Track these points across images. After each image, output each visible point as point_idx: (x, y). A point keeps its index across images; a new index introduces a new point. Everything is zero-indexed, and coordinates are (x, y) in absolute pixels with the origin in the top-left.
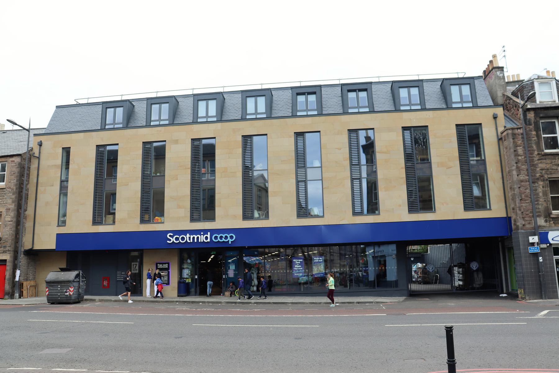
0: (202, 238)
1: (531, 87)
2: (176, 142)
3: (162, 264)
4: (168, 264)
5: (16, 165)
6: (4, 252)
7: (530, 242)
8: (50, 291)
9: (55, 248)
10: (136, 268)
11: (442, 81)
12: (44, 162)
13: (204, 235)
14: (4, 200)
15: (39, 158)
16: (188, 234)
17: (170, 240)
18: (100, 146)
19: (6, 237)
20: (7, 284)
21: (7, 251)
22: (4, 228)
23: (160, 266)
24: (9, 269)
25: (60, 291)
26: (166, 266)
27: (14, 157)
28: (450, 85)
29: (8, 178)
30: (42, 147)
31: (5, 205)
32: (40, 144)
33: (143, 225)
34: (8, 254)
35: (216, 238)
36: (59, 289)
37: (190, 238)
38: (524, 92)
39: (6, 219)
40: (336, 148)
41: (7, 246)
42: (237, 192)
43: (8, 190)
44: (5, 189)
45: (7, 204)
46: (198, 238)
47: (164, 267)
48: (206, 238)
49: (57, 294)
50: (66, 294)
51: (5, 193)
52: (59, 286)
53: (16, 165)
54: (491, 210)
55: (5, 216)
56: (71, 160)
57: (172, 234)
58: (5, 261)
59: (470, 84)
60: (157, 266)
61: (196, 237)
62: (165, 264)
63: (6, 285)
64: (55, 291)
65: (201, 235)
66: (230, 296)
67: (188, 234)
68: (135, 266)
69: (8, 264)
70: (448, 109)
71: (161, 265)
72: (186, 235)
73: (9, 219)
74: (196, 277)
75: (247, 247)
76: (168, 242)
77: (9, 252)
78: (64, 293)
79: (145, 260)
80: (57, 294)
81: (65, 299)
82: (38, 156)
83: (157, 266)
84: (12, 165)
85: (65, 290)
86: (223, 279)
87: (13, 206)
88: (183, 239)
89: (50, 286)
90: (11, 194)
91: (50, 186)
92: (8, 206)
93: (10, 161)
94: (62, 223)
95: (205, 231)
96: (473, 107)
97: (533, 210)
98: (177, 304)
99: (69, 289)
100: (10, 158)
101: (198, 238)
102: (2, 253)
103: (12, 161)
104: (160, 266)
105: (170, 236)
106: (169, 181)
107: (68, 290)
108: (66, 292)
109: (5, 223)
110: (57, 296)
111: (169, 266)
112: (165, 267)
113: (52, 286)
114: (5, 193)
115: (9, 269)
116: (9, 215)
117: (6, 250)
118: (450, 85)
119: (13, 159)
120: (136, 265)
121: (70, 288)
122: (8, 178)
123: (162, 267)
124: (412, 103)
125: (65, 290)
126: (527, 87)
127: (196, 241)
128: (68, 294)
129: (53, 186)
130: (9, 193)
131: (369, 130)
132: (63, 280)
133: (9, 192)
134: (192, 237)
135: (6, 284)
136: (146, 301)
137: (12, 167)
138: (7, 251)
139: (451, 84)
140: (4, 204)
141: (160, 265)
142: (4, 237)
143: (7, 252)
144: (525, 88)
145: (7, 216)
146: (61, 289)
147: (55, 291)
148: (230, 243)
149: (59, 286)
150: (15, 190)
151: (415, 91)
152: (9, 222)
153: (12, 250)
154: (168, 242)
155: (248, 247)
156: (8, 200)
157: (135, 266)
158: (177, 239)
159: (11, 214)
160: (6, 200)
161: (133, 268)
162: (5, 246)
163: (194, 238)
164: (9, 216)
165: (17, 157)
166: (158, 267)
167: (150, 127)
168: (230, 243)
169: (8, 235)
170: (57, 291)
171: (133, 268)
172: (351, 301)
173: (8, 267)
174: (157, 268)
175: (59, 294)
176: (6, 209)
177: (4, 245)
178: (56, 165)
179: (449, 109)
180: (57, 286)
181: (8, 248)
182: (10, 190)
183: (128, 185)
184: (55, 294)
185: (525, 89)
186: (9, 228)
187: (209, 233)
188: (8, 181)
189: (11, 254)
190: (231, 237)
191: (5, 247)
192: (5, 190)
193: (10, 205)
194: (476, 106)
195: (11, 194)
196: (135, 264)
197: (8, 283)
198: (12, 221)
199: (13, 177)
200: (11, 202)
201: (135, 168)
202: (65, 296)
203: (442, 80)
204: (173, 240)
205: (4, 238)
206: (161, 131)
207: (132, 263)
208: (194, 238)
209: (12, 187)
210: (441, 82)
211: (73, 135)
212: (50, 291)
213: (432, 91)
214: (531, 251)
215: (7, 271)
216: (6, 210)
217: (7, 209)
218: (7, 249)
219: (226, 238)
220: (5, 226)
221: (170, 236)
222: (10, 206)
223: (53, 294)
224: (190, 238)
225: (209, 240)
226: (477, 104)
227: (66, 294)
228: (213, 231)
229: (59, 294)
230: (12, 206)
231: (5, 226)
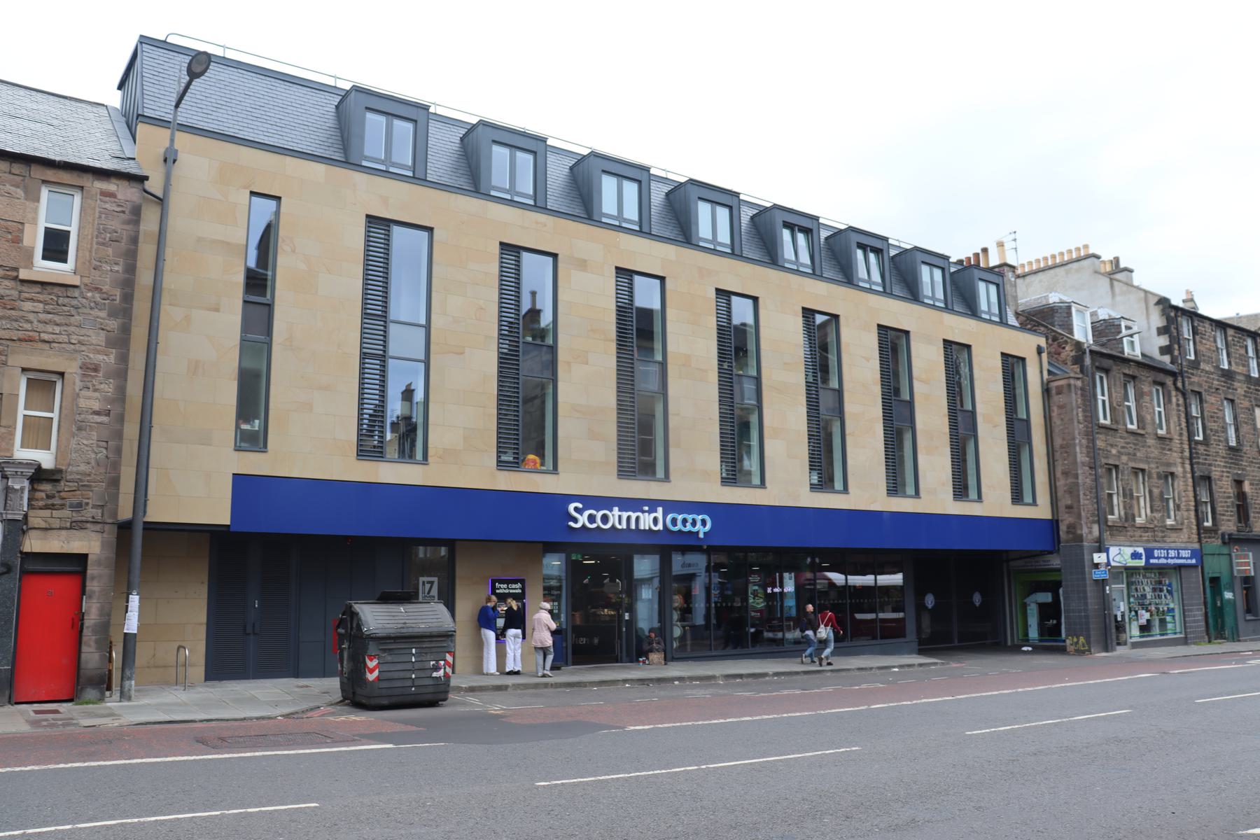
0: (646, 521)
1: (1067, 313)
2: (582, 264)
3: (508, 582)
4: (522, 582)
5: (123, 212)
6: (77, 525)
7: (1096, 561)
8: (385, 668)
9: (229, 523)
10: (431, 594)
11: (469, 130)
12: (181, 222)
13: (650, 512)
14: (72, 329)
15: (161, 201)
16: (616, 509)
17: (576, 520)
18: (376, 221)
19: (83, 468)
20: (92, 644)
21: (87, 522)
22: (73, 435)
23: (502, 589)
24: (97, 589)
25: (417, 666)
26: (516, 588)
27: (114, 180)
28: (367, 108)
29: (90, 252)
30: (177, 170)
31: (76, 351)
32: (169, 159)
33: (506, 473)
34: (93, 534)
35: (674, 521)
36: (413, 660)
37: (620, 517)
38: (1056, 318)
39: (83, 403)
40: (863, 357)
41: (87, 504)
42: (710, 419)
43: (89, 294)
44: (76, 290)
45: (83, 348)
46: (637, 519)
47: (511, 591)
48: (655, 521)
49: (407, 675)
50: (435, 674)
51: (74, 302)
52: (414, 651)
53: (123, 212)
54: (1037, 505)
55: (77, 390)
56: (283, 241)
57: (580, 506)
58: (82, 558)
59: (415, 121)
60: (494, 589)
61: (634, 516)
62: (515, 581)
63: (84, 649)
64: (400, 667)
65: (643, 512)
66: (663, 662)
67: (616, 509)
68: (428, 586)
69: (91, 570)
70: (884, 294)
71: (505, 586)
72: (611, 511)
73: (96, 406)
74: (627, 616)
75: (705, 547)
76: (571, 524)
77: (98, 527)
78: (427, 673)
79: (460, 572)
80: (407, 675)
81: (431, 690)
82: (160, 194)
83: (494, 589)
84: (107, 206)
85: (432, 663)
86: (624, 624)
87: (112, 357)
88: (605, 519)
89: (384, 650)
90: (103, 314)
91: (209, 309)
92: (91, 356)
93: (99, 191)
94: (254, 441)
95: (653, 504)
96: (414, 177)
97: (1098, 515)
98: (628, 687)
99: (445, 660)
100: (97, 180)
101: (637, 519)
102: (67, 529)
103: (104, 194)
104: (502, 589)
105: (576, 509)
106: (569, 363)
107: (442, 663)
108: (437, 669)
109: (78, 417)
110: (409, 683)
111: (523, 589)
112: (514, 591)
113: (390, 649)
114: (74, 302)
115: (97, 589)
116: (96, 390)
117: (84, 519)
118: (367, 108)
119: (111, 186)
120: (432, 583)
121: (447, 655)
122: (90, 252)
123: (507, 591)
124: (517, 190)
125: (432, 663)
126: (1059, 311)
127: (633, 526)
128: (441, 673)
129: (217, 310)
130: (91, 308)
131: (527, 254)
132: (425, 630)
133: (92, 305)
134: (625, 515)
135: (89, 646)
136: (552, 684)
137: (107, 213)
138: (87, 522)
139: (924, 261)
140: (72, 346)
141: (502, 586)
142: (75, 469)
143: (88, 525)
144: (1057, 312)
145: (84, 393)
146: (419, 659)
147: (400, 667)
148: (701, 535)
149: (414, 651)
150: (118, 302)
151: (404, 129)
152: (96, 417)
153: (110, 521)
154: (571, 524)
155: (708, 546)
156: (90, 332)
157: (428, 586)
158: (592, 519)
159: (102, 386)
160: (83, 332)
161: (423, 593)
162: (80, 505)
163: (629, 518)
164: (97, 394)
165: (125, 183)
166: (497, 591)
167: (647, 236)
168: (701, 535)
169: (93, 462)
170: (409, 666)
171: (423, 593)
172: (710, 673)
173: (95, 583)
174: (493, 592)
175: (413, 676)
176: (79, 363)
177: (75, 501)
178: (228, 244)
179: (743, 259)
180: (407, 651)
181: (89, 513)
182: (97, 296)
183: (462, 353)
184: (402, 675)
185: (1057, 315)
186: (95, 438)
187: (660, 510)
188: (90, 262)
189: (105, 535)
190: (704, 523)
191: (79, 506)
192: (76, 293)
193: (98, 352)
194: (424, 178)
195: (103, 314)
196: (428, 582)
197: (97, 642)
198: (108, 413)
199: (110, 251)
200: (104, 344)
201: (482, 309)
202: (429, 682)
203: (469, 128)
204: (583, 520)
205: (72, 473)
206: (545, 226)
207: (421, 579)
208: (629, 518)
209: (106, 288)
210: (466, 130)
211: (289, 160)
212: (385, 668)
213: (443, 145)
214: (1095, 577)
215: (90, 597)
216: (81, 368)
217: (84, 367)
218: (89, 515)
219: (694, 523)
220: (80, 429)
221: (576, 509)
222: (101, 357)
223: (396, 675)
224: (620, 517)
225: (660, 527)
226: (426, 177)
227: (435, 674)
228: (671, 506)
229: (413, 676)
230: (105, 357)
231: (80, 429)
